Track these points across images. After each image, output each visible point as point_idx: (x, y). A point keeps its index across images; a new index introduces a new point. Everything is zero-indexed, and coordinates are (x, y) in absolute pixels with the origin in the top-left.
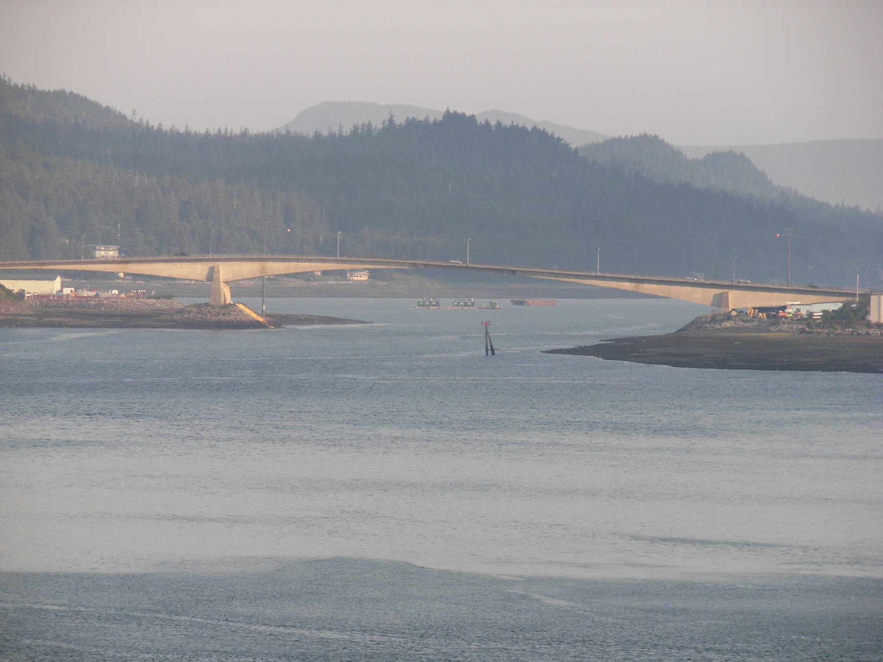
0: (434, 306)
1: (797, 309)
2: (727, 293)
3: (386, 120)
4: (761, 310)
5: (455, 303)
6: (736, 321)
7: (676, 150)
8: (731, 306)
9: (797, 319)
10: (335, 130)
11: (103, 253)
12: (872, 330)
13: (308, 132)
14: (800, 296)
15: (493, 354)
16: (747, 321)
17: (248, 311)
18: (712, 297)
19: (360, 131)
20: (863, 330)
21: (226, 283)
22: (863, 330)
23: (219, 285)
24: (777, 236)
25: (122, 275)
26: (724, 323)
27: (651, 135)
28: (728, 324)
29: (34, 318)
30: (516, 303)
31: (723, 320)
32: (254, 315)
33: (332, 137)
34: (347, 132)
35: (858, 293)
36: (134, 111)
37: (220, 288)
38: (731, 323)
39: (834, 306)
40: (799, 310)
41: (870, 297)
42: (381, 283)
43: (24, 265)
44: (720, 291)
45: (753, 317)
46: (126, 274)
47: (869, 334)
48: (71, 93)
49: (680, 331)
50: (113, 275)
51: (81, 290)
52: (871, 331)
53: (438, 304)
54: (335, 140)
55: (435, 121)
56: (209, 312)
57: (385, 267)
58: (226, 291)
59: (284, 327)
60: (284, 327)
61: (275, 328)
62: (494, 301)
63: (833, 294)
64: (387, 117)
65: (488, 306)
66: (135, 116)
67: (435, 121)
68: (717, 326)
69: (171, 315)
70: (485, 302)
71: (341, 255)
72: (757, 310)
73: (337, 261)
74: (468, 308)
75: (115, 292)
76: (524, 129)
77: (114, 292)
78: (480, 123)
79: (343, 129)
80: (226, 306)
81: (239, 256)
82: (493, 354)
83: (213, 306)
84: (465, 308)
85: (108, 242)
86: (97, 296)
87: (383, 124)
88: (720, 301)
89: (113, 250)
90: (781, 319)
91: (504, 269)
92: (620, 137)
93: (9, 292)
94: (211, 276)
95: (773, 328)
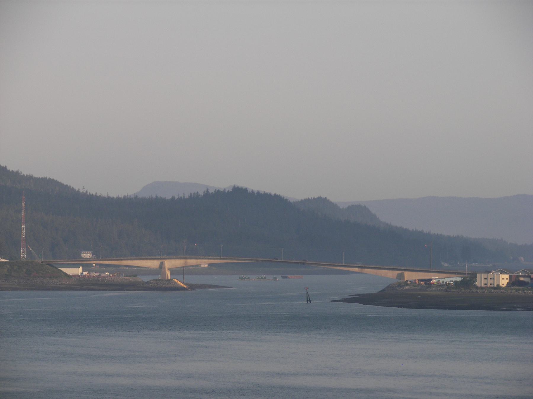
0: (247, 279)
1: (438, 280)
2: (404, 273)
3: (205, 191)
4: (422, 280)
5: (257, 278)
6: (410, 286)
7: (335, 204)
8: (406, 279)
9: (439, 285)
10: (182, 196)
11: (85, 254)
12: (479, 290)
13: (147, 195)
14: (438, 274)
15: (310, 302)
16: (416, 286)
17: (179, 283)
18: (396, 274)
19: (192, 196)
20: (475, 291)
21: (169, 269)
22: (474, 290)
23: (165, 270)
24: (426, 246)
25: (94, 265)
26: (405, 287)
27: (323, 198)
28: (407, 287)
29: (79, 287)
30: (283, 277)
31: (404, 286)
32: (182, 284)
33: (180, 199)
34: (187, 196)
35: (466, 273)
36: (84, 187)
37: (165, 272)
38: (408, 287)
39: (459, 279)
40: (439, 281)
41: (477, 275)
42: (214, 268)
43: (73, 261)
44: (400, 272)
45: (418, 284)
46: (96, 264)
47: (478, 292)
48: (50, 179)
49: (382, 291)
50: (91, 265)
51: (92, 273)
52: (478, 291)
53: (249, 278)
54: (181, 200)
55: (228, 191)
56: (161, 283)
57: (243, 262)
58: (168, 273)
59: (195, 290)
60: (195, 290)
61: (191, 290)
62: (275, 276)
63: (458, 273)
64: (206, 190)
65: (273, 279)
66: (84, 189)
67: (228, 191)
68: (402, 288)
69: (142, 284)
70: (271, 277)
71: (223, 256)
72: (420, 281)
73: (221, 259)
74: (263, 280)
75: (107, 273)
76: (270, 194)
77: (107, 273)
78: (250, 192)
79: (185, 195)
80: (168, 280)
81: (167, 257)
82: (310, 302)
83: (162, 280)
84: (262, 280)
85: (87, 250)
86: (99, 275)
87: (204, 193)
88: (401, 276)
89: (90, 253)
90: (432, 285)
91: (299, 262)
92: (309, 198)
93: (66, 274)
94: (162, 266)
95: (428, 289)
